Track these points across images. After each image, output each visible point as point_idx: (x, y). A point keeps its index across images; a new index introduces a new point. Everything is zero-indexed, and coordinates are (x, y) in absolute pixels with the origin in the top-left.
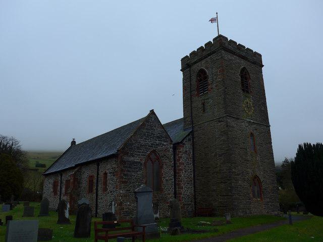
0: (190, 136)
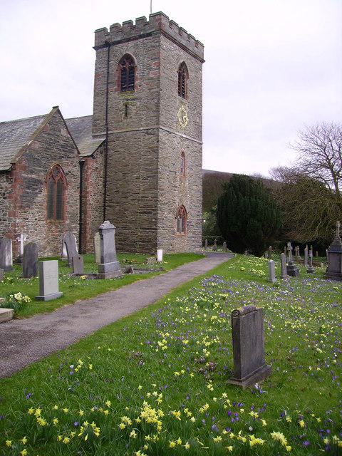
0: (103, 147)
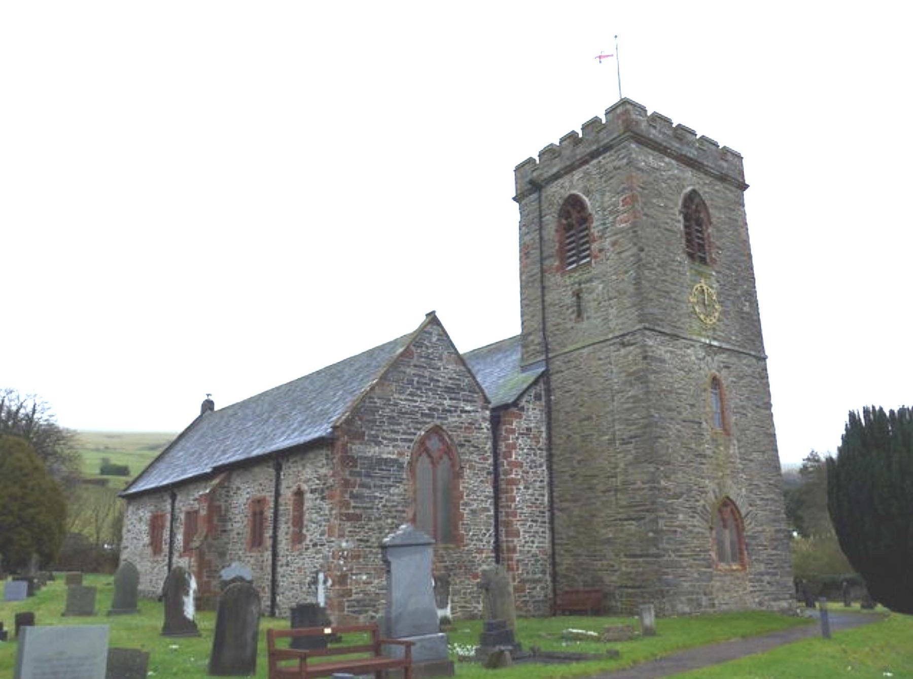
0: (541, 387)
